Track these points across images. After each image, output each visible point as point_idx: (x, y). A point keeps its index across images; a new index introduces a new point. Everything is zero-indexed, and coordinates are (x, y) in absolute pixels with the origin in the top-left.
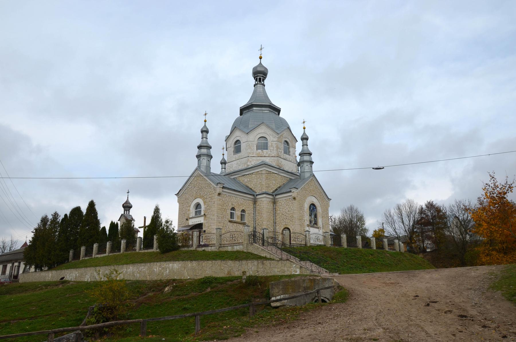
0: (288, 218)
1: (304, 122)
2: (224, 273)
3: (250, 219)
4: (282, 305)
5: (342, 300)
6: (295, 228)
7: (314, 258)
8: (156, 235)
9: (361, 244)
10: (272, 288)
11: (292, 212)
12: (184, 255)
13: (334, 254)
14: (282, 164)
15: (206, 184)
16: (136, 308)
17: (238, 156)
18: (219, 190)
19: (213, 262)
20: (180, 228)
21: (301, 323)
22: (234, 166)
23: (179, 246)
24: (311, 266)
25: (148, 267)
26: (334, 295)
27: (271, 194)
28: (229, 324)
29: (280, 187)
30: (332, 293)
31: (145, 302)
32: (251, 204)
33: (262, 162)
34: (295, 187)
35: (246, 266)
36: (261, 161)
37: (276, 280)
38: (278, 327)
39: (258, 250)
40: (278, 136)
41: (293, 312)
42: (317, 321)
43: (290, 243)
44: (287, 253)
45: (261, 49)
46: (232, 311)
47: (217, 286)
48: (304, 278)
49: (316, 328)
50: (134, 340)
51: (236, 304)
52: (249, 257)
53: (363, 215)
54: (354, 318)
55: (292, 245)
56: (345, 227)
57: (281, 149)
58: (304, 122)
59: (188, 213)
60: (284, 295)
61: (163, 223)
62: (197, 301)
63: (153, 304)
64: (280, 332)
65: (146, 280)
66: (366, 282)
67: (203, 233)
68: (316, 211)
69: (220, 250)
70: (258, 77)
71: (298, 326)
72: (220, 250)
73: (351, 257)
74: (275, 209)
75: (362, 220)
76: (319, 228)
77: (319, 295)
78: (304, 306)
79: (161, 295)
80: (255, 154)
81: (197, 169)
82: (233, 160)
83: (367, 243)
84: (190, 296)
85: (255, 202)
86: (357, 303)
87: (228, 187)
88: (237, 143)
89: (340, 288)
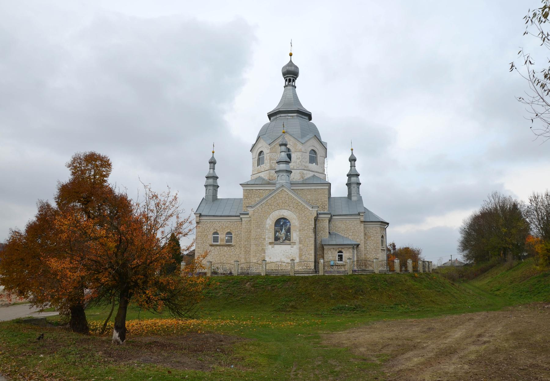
70: (288, 78)
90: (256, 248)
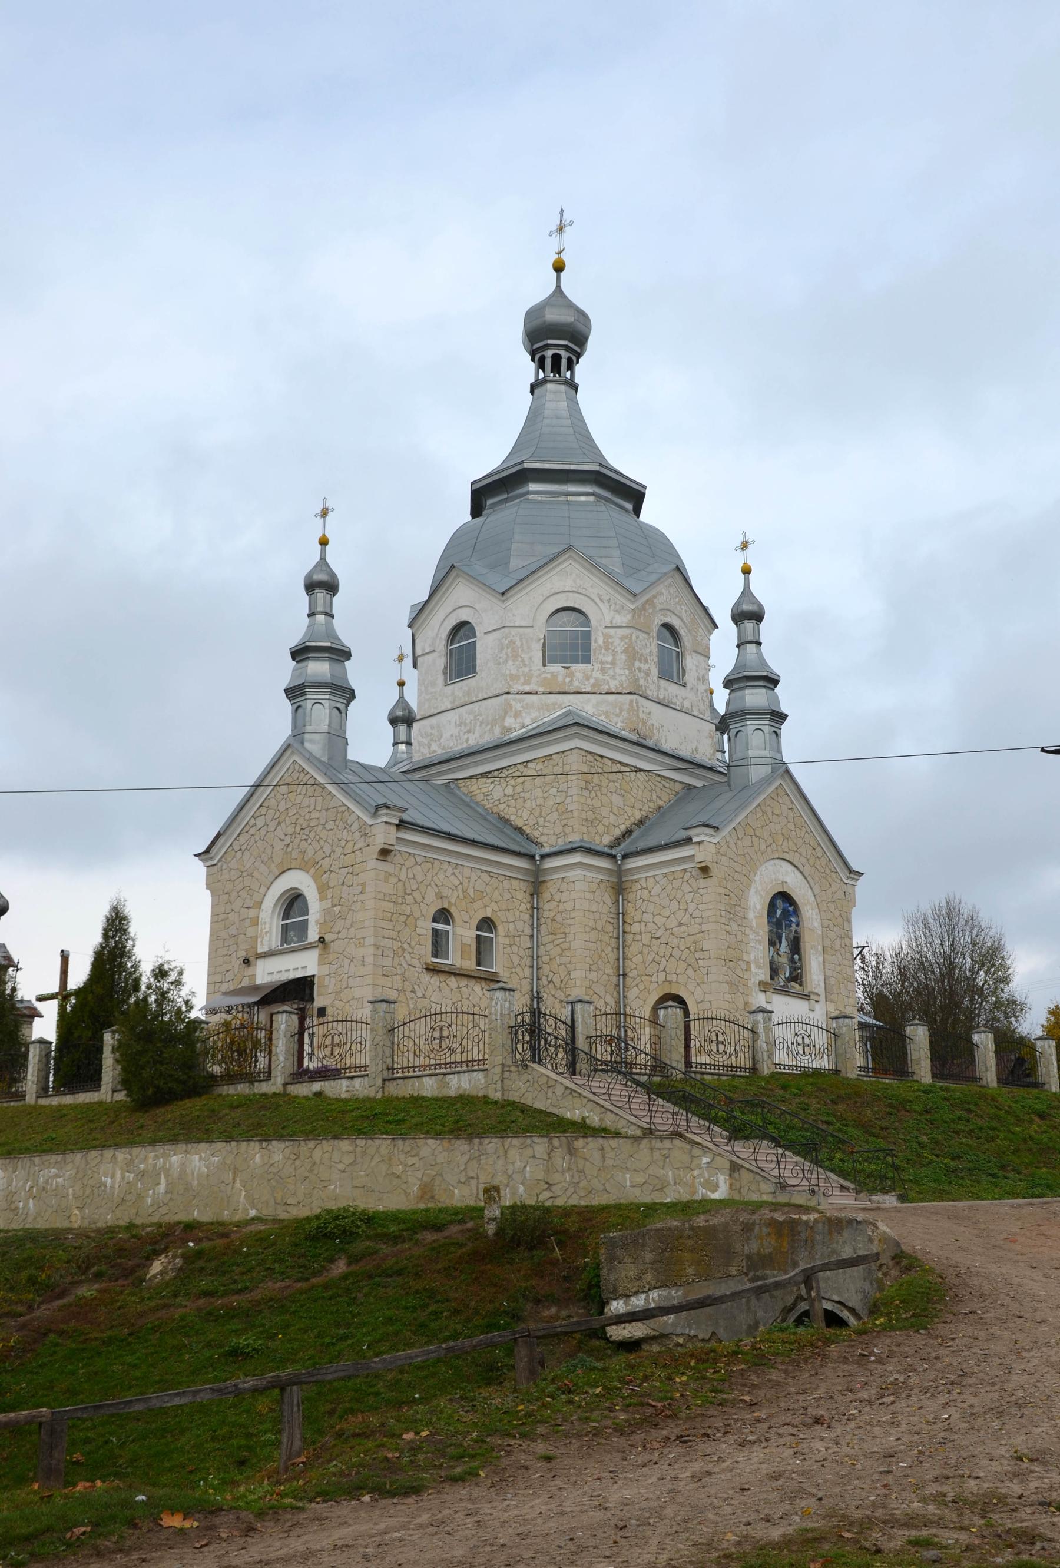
0: (676, 953)
1: (745, 546)
2: (407, 1195)
3: (516, 959)
4: (653, 1333)
5: (913, 1315)
6: (708, 998)
7: (791, 1127)
8: (114, 1028)
9: (994, 1069)
10: (612, 1258)
11: (694, 929)
12: (233, 1115)
13: (876, 1109)
14: (650, 722)
15: (327, 810)
16: (21, 1357)
17: (461, 689)
18: (383, 834)
19: (357, 1146)
20: (218, 996)
21: (737, 1420)
22: (446, 734)
23: (213, 1077)
24: (778, 1163)
25: (78, 1172)
26: (878, 1295)
27: (606, 850)
28: (429, 1423)
29: (641, 822)
30: (872, 1284)
31: (62, 1326)
32: (520, 895)
33: (568, 714)
34: (709, 822)
35: (501, 1162)
36: (564, 710)
37: (627, 1224)
38: (638, 1438)
39: (550, 1094)
40: (633, 602)
41: (701, 1367)
42: (805, 1409)
43: (688, 1063)
44: (674, 1104)
45: (561, 229)
46: (439, 1360)
47: (376, 1252)
48: (749, 1217)
49: (805, 1446)
50: (8, 1509)
51: (455, 1330)
52: (513, 1122)
53: (999, 941)
54: (968, 1403)
55: (695, 1073)
56: (923, 991)
57: (646, 661)
58: (745, 546)
59: (250, 932)
60: (664, 1292)
61: (144, 979)
62: (288, 1317)
63: (97, 1335)
64: (645, 1457)
65: (69, 1230)
66: (1018, 1238)
67: (315, 1019)
68: (798, 925)
69: (386, 1093)
70: (549, 353)
71: (726, 1433)
72: (386, 1093)
73: (952, 1125)
74: (620, 916)
75: (997, 963)
76: (812, 997)
77: (813, 1294)
78: (748, 1341)
79: (133, 1294)
80: (534, 679)
81: (289, 745)
82: (443, 709)
83: (1021, 1061)
84: (257, 1295)
85: (536, 885)
86: (982, 1335)
87: (420, 823)
88: (461, 632)
89: (905, 1262)
90: (728, 997)
